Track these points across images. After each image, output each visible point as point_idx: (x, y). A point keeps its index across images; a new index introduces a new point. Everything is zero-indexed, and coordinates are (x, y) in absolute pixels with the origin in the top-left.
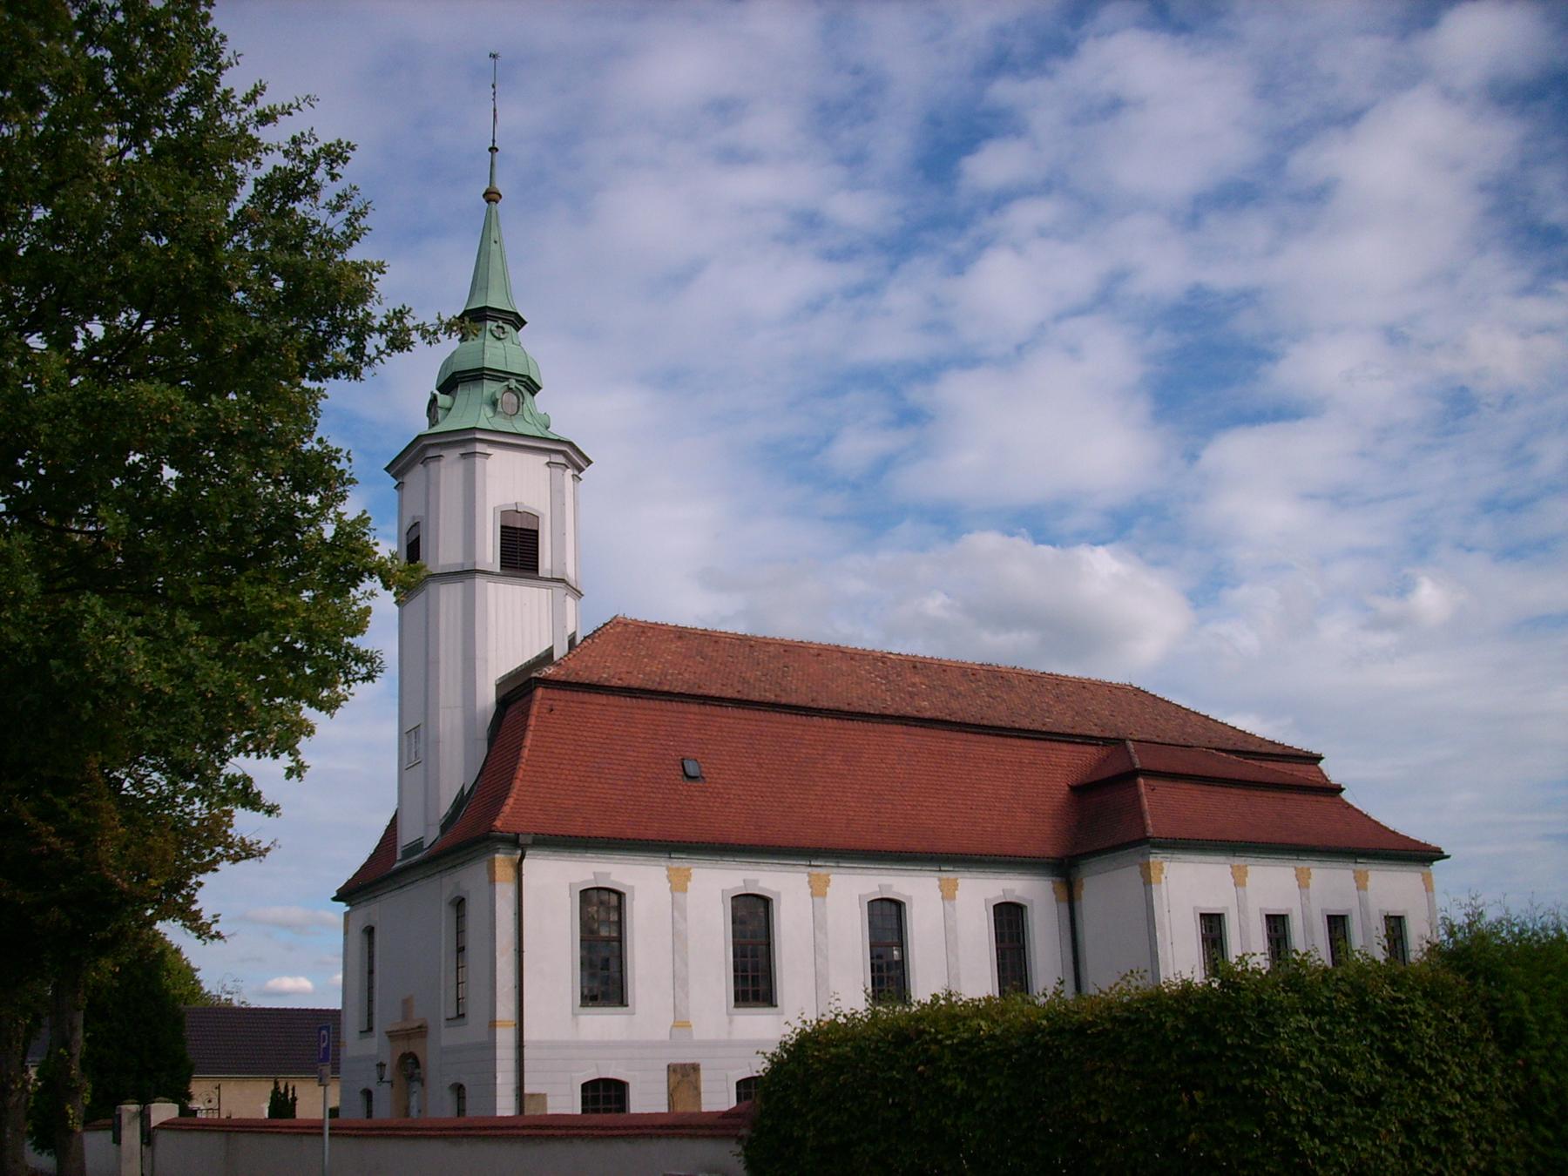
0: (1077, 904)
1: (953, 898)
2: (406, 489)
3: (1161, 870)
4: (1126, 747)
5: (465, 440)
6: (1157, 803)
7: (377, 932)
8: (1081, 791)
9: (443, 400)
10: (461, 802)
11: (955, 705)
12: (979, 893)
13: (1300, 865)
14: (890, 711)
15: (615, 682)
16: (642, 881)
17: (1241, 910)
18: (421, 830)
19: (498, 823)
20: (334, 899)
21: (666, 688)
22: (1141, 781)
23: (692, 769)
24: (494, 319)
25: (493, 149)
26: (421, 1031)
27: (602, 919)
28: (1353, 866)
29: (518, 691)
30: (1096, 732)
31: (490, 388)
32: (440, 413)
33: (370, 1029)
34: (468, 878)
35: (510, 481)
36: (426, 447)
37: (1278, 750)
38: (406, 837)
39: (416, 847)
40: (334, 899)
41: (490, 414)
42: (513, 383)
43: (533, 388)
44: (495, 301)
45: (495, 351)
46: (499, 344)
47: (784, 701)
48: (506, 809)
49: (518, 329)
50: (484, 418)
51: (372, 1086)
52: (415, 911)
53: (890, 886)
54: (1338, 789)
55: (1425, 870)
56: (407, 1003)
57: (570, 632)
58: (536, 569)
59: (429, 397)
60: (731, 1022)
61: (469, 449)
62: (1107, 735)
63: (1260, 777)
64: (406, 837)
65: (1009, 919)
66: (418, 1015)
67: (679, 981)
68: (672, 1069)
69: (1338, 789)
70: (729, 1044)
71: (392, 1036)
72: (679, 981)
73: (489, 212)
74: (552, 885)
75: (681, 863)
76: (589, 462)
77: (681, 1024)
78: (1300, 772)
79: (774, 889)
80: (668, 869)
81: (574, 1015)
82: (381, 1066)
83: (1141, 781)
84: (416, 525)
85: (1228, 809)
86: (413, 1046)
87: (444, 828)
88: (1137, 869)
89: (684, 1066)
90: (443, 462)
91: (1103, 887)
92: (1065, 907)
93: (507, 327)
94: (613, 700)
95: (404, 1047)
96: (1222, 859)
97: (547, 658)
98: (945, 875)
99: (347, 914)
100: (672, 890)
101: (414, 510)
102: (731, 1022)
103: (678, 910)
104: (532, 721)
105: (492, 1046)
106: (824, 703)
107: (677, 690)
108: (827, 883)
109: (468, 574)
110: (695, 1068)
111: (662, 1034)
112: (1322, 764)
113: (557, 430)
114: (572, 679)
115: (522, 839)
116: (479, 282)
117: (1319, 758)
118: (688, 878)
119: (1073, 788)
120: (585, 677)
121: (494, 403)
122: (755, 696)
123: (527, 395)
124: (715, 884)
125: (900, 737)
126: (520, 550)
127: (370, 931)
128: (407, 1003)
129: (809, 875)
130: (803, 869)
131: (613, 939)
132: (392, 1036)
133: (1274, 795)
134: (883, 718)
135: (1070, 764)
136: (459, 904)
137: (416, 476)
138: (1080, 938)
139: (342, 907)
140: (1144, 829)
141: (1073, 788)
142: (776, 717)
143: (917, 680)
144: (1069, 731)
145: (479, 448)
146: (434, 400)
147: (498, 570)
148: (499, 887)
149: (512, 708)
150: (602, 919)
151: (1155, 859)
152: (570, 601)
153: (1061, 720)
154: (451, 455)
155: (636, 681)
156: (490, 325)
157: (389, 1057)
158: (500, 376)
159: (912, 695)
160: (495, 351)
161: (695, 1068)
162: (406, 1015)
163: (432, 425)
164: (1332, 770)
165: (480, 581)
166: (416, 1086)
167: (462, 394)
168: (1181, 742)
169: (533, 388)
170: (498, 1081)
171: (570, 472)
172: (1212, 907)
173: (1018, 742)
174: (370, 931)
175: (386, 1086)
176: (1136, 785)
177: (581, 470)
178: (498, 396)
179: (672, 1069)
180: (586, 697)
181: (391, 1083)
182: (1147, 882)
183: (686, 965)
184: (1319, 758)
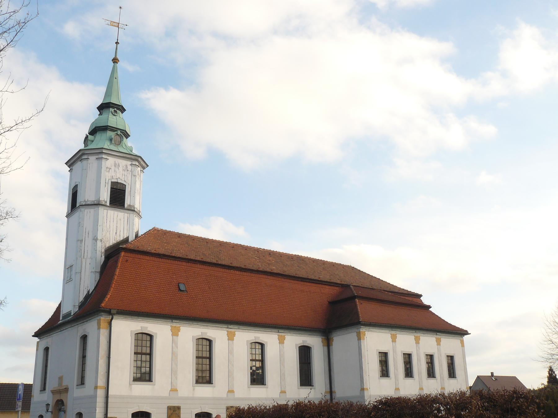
0: (331, 347)
1: (283, 343)
2: (73, 170)
3: (365, 335)
4: (350, 288)
5: (99, 152)
6: (364, 309)
7: (50, 350)
8: (333, 303)
9: (90, 137)
10: (88, 296)
11: (285, 269)
12: (294, 341)
13: (416, 335)
14: (261, 269)
15: (153, 251)
16: (161, 330)
17: (394, 351)
18: (70, 308)
19: (103, 305)
20: (33, 336)
21: (174, 255)
22: (357, 300)
23: (182, 287)
24: (113, 108)
25: (117, 43)
26: (66, 390)
27: (144, 346)
28: (436, 336)
29: (114, 253)
30: (339, 282)
31: (110, 134)
32: (89, 142)
33: (44, 389)
34: (90, 327)
35: (113, 170)
36: (102, 153)
37: (406, 292)
38: (64, 311)
39: (69, 314)
40: (33, 336)
41: (109, 144)
42: (119, 132)
43: (127, 136)
44: (114, 100)
45: (112, 120)
46: (114, 117)
47: (220, 263)
48: (107, 299)
49: (122, 113)
50: (107, 145)
51: (43, 414)
52: (67, 341)
53: (259, 337)
54: (429, 307)
55: (461, 338)
56: (61, 378)
57: (136, 231)
58: (124, 206)
59: (85, 136)
60: (194, 390)
61: (100, 156)
62: (343, 283)
63: (400, 301)
64: (64, 311)
65: (305, 353)
66: (65, 383)
67: (174, 372)
68: (169, 408)
69: (429, 307)
70: (193, 399)
71: (53, 392)
72: (174, 372)
73: (114, 67)
74: (124, 330)
75: (176, 324)
76: (148, 166)
77: (174, 390)
78: (415, 300)
79: (213, 336)
80: (171, 326)
81: (130, 385)
82: (48, 405)
83: (357, 300)
84: (76, 186)
85: (389, 312)
86: (63, 397)
87: (80, 307)
88: (355, 334)
89: (174, 407)
90: (89, 161)
91: (342, 340)
92: (326, 348)
93: (118, 111)
94: (152, 258)
95: (58, 397)
96: (387, 331)
97: (126, 241)
98: (280, 334)
99: (38, 343)
100: (172, 335)
101: (77, 180)
102: (194, 390)
103: (176, 342)
104: (119, 265)
105: (95, 397)
106: (235, 264)
107: (178, 256)
108: (234, 335)
109: (98, 204)
110: (179, 408)
111: (165, 393)
112: (422, 298)
113: (135, 152)
114: (136, 249)
115: (113, 311)
116: (108, 93)
117: (421, 296)
118: (179, 330)
119: (329, 303)
120: (141, 249)
121: (111, 140)
122: (208, 260)
123: (124, 138)
124: (190, 333)
125: (270, 280)
126: (118, 197)
127: (47, 349)
128: (61, 378)
129: (278, 335)
130: (225, 329)
131: (206, 358)
132: (53, 392)
133: (405, 310)
134: (258, 272)
135: (329, 292)
136: (84, 338)
137: (78, 165)
138: (332, 360)
139: (36, 339)
140: (359, 319)
141: (329, 303)
142: (217, 269)
143: (271, 259)
144: (328, 281)
145: (104, 156)
146: (87, 137)
147: (108, 204)
148: (102, 331)
149: (111, 260)
150: (144, 346)
151: (363, 329)
152: (136, 219)
153: (325, 277)
154: (92, 158)
155: (162, 251)
156: (112, 110)
157: (51, 402)
158: (113, 129)
159: (269, 264)
160: (112, 120)
161: (179, 408)
162: (60, 383)
163: (85, 146)
164: (425, 300)
165: (101, 210)
166: (62, 413)
167: (98, 136)
168: (370, 287)
169: (127, 136)
170: (97, 411)
171: (139, 169)
172: (384, 350)
173: (309, 284)
174: (47, 349)
175: (49, 414)
176: (355, 302)
177: (144, 168)
178: (113, 137)
179: (169, 408)
180: (142, 257)
181: (52, 412)
182: (359, 339)
183: (177, 366)
184: (421, 296)
